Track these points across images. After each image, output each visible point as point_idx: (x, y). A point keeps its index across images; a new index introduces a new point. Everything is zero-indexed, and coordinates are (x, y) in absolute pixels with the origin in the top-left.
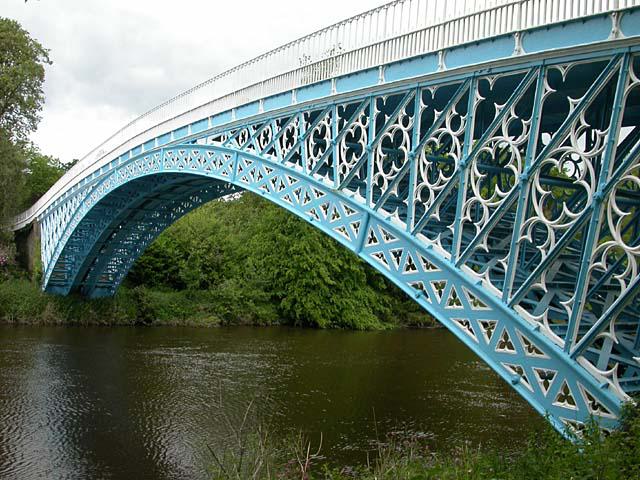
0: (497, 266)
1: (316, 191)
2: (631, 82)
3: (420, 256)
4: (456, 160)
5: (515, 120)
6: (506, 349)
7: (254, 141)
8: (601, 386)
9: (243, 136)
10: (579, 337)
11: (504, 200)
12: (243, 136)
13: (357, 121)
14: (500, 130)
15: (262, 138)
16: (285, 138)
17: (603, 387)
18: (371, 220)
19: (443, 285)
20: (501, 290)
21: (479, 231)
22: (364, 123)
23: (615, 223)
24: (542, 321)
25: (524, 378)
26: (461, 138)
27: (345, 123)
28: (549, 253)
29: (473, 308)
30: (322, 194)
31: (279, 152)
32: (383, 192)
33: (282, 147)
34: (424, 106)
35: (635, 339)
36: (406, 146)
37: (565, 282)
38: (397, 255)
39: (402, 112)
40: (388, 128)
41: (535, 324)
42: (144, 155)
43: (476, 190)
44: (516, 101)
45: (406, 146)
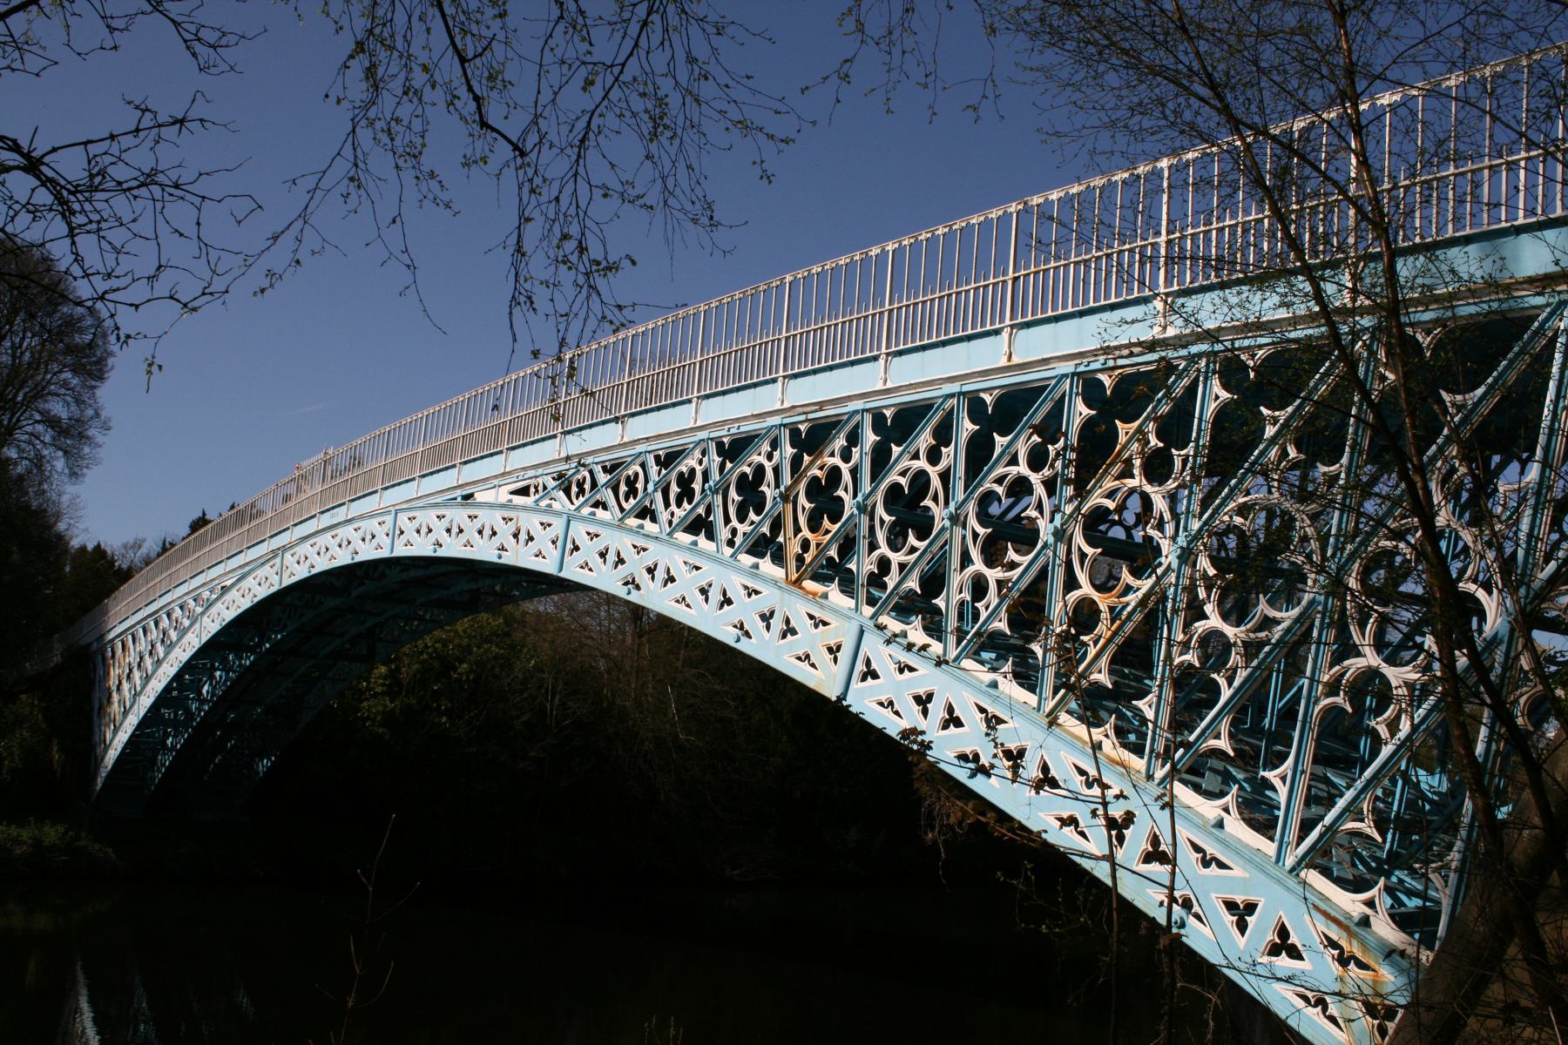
1: (811, 617)
2: (1217, 397)
4: (1165, 545)
5: (1157, 450)
7: (608, 496)
9: (580, 485)
10: (1301, 839)
11: (1020, 569)
12: (580, 485)
13: (832, 455)
15: (623, 488)
16: (675, 489)
21: (1092, 652)
22: (770, 457)
24: (1226, 810)
25: (1197, 917)
26: (1050, 485)
27: (807, 458)
28: (1236, 683)
31: (664, 516)
32: (891, 586)
34: (1086, 411)
36: (935, 499)
37: (1260, 738)
39: (925, 440)
40: (993, 475)
43: (975, 554)
45: (935, 499)
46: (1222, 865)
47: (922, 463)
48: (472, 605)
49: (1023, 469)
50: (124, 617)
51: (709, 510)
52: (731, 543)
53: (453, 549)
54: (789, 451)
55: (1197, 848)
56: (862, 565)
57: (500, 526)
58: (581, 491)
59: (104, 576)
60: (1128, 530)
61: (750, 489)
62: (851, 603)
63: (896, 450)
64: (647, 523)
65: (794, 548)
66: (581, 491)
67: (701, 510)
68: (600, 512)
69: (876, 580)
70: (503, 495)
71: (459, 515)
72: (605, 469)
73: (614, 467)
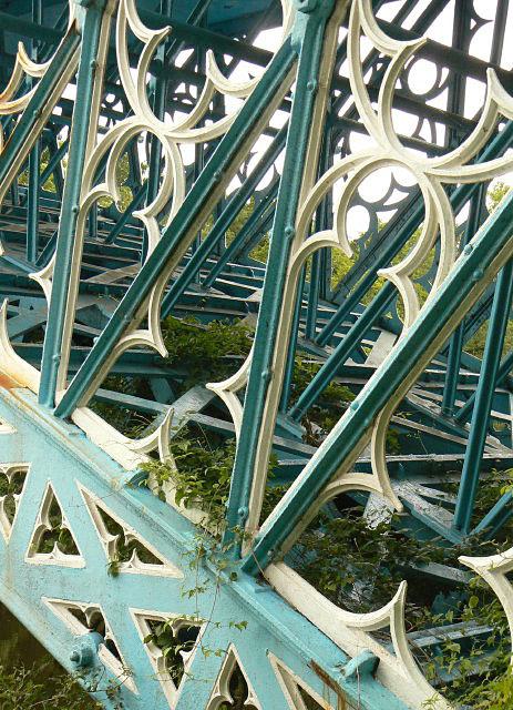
0: (206, 411)
8: (350, 668)
17: (354, 677)
19: (188, 635)
20: (423, 648)
23: (133, 61)
25: (111, 646)
28: (164, 230)
35: (456, 500)
41: (361, 648)
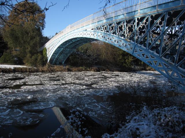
3: (150, 55)
6: (147, 58)
9: (99, 28)
12: (99, 28)
14: (174, 24)
16: (111, 29)
18: (136, 47)
27: (128, 24)
29: (152, 58)
30: (130, 45)
33: (110, 30)
34: (168, 17)
38: (143, 55)
42: (73, 33)
44: (180, 17)
46: (154, 58)
47: (132, 24)
48: (86, 42)
49: (158, 25)
50: (47, 45)
51: (115, 31)
52: (118, 35)
53: (85, 36)
54: (126, 23)
55: (151, 56)
56: (136, 38)
57: (90, 33)
58: (99, 29)
59: (47, 40)
60: (169, 32)
61: (121, 28)
62: (134, 42)
63: (140, 23)
64: (114, 35)
65: (118, 34)
66: (99, 29)
67: (114, 31)
68: (102, 31)
69: (137, 39)
70: (90, 30)
71: (85, 32)
72: (102, 26)
73: (104, 26)
